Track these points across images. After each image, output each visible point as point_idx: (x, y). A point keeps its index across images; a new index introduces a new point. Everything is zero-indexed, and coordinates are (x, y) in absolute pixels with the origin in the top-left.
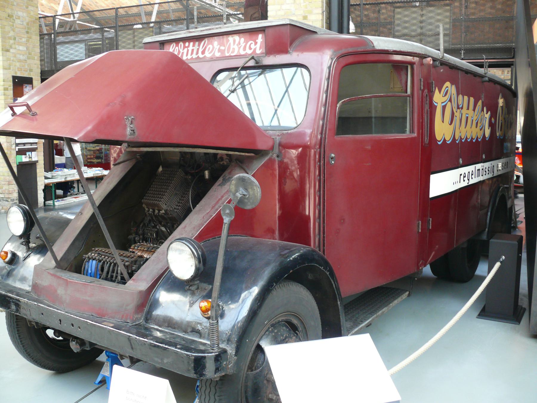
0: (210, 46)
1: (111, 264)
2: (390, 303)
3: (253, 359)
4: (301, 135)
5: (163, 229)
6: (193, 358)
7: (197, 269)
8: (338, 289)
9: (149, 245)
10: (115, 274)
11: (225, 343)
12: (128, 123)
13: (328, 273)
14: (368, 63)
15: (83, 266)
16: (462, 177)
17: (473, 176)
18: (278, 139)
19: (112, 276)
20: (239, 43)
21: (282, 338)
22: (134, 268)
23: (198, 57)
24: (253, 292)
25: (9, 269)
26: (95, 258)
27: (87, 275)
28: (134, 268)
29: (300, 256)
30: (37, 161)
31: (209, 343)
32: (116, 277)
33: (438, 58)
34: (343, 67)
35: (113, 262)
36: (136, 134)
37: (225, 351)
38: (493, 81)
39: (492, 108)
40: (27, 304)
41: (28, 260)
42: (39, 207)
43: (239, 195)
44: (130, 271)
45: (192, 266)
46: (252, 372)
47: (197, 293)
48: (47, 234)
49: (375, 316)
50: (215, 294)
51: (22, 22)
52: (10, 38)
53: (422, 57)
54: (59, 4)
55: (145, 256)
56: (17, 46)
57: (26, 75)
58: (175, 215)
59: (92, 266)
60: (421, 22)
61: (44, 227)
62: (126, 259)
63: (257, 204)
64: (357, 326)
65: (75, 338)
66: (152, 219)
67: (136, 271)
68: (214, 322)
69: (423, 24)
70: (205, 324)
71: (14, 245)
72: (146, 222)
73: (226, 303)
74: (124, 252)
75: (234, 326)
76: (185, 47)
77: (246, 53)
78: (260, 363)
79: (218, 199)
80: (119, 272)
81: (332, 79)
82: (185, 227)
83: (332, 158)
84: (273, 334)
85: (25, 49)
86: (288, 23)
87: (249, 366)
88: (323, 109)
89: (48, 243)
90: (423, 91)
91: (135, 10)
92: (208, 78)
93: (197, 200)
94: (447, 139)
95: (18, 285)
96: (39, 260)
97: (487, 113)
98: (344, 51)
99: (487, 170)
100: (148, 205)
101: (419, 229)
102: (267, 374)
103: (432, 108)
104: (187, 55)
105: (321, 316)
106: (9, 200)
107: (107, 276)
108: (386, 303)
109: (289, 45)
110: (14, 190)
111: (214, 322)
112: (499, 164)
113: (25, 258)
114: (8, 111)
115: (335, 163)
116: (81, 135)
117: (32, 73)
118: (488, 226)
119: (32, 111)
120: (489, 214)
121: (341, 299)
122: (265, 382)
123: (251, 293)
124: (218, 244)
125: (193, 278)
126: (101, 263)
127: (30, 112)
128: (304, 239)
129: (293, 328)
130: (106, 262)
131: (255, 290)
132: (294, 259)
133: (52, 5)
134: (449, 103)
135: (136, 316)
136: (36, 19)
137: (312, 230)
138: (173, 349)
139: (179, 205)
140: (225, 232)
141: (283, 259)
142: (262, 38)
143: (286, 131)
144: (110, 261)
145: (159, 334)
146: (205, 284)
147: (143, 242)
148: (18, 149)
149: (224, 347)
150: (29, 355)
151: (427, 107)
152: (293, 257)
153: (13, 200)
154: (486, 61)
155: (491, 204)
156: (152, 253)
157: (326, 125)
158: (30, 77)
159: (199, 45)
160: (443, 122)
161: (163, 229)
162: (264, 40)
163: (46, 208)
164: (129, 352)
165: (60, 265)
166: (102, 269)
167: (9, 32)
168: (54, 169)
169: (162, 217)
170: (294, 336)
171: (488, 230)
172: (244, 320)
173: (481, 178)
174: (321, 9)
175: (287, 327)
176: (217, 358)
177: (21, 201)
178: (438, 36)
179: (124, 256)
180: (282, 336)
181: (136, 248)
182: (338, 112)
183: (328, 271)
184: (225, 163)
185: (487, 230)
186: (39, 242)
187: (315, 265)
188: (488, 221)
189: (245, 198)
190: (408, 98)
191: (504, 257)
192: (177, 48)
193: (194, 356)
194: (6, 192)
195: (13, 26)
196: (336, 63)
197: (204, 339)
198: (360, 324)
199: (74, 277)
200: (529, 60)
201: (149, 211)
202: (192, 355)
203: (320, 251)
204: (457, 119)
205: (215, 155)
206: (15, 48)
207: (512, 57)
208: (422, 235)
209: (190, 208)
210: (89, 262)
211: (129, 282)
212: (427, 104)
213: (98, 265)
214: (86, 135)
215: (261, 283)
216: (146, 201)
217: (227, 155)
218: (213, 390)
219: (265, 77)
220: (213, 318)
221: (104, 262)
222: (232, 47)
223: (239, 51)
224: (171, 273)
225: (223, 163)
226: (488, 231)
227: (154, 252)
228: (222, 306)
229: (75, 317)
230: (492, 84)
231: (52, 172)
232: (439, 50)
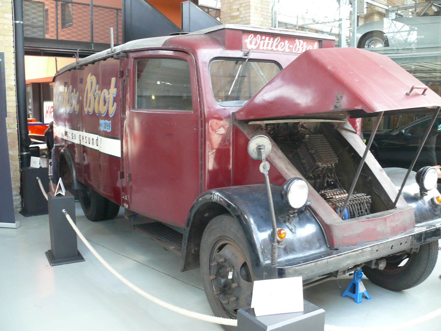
0: (282, 43)
20: (302, 46)
23: (272, 49)
76: (261, 40)
77: (278, 50)
104: (263, 46)
159: (273, 40)
192: (255, 39)
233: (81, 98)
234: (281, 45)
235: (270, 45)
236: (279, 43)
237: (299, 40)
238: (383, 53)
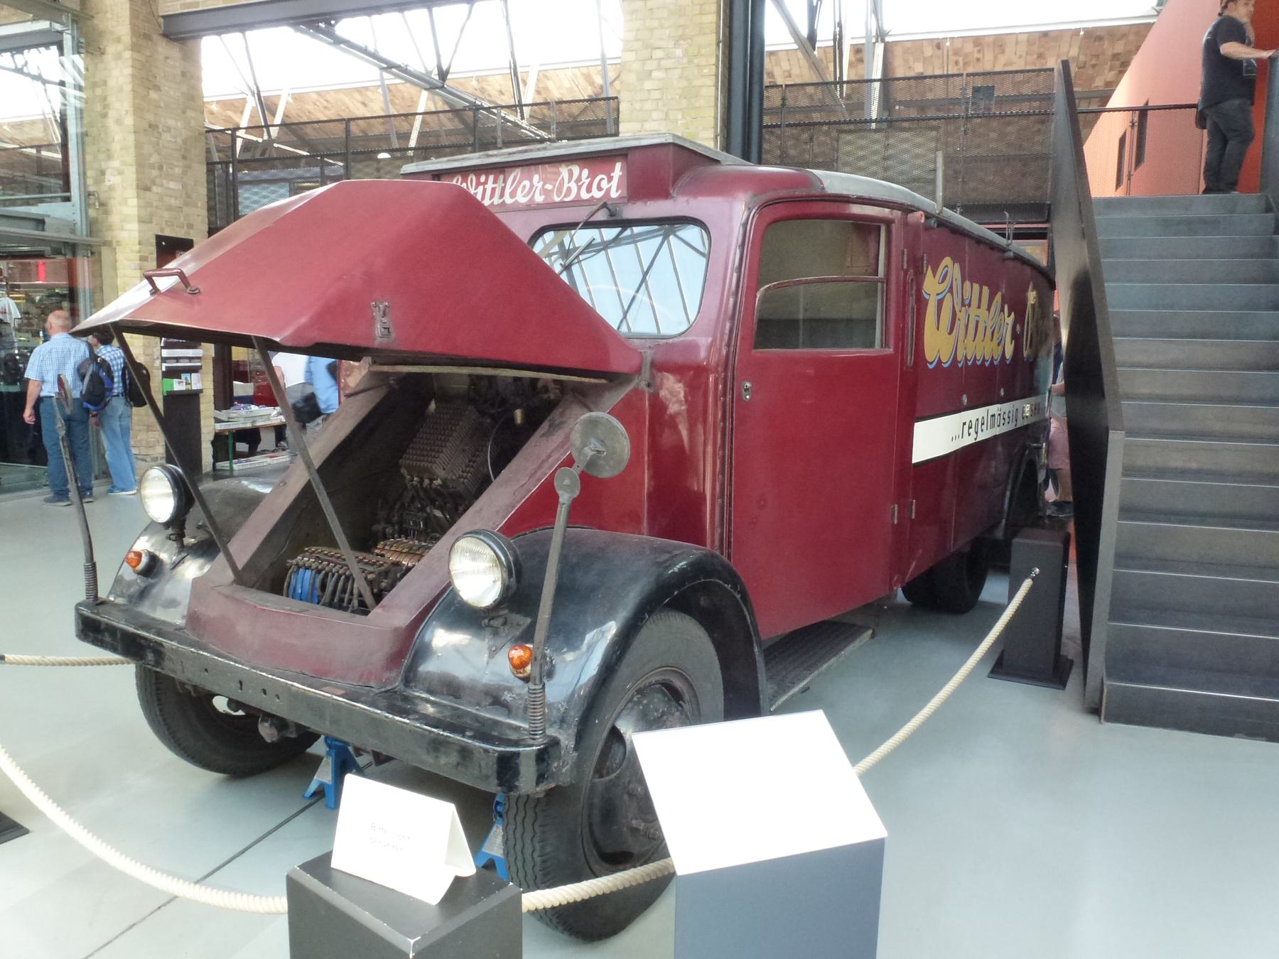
1: (340, 576)
2: (841, 650)
3: (605, 754)
4: (692, 347)
5: (438, 513)
6: (496, 755)
7: (506, 589)
8: (755, 627)
9: (411, 542)
10: (347, 596)
11: (556, 726)
12: (377, 314)
13: (738, 597)
14: (812, 218)
15: (287, 580)
16: (966, 427)
17: (984, 427)
18: (649, 355)
19: (342, 600)
20: (579, 179)
22: (383, 585)
24: (609, 630)
25: (143, 585)
26: (310, 566)
27: (288, 596)
28: (383, 585)
29: (692, 565)
30: (201, 391)
31: (526, 726)
32: (350, 601)
33: (933, 213)
34: (770, 224)
35: (344, 574)
36: (393, 335)
37: (555, 743)
38: (1020, 259)
39: (1017, 306)
40: (176, 651)
41: (181, 568)
42: (204, 472)
43: (589, 452)
44: (375, 590)
45: (495, 582)
46: (602, 779)
47: (504, 631)
48: (218, 520)
49: (816, 672)
50: (541, 633)
51: (175, 137)
52: (152, 167)
53: (907, 209)
54: (242, 112)
55: (404, 562)
56: (164, 182)
57: (180, 234)
58: (460, 489)
59: (304, 580)
60: (885, 159)
61: (213, 508)
62: (370, 568)
63: (622, 467)
64: (785, 692)
65: (268, 716)
66: (419, 495)
67: (389, 591)
68: (537, 687)
69: (890, 163)
70: (518, 691)
71: (153, 540)
72: (407, 500)
73: (558, 650)
74: (364, 554)
75: (573, 694)
76: (478, 184)
77: (592, 197)
78: (617, 761)
79: (540, 461)
80: (355, 591)
82: (481, 510)
83: (746, 390)
84: (641, 707)
85: (181, 187)
86: (671, 141)
87: (596, 767)
88: (731, 300)
89: (220, 537)
90: (906, 272)
91: (378, 129)
92: (524, 236)
93: (502, 461)
94: (944, 360)
95: (161, 614)
96: (201, 568)
97: (1009, 316)
98: (770, 195)
99: (1006, 417)
100: (409, 468)
101: (893, 519)
102: (629, 782)
103: (921, 303)
105: (723, 674)
106: (149, 459)
107: (332, 599)
108: (834, 651)
109: (671, 183)
110: (158, 442)
111: (537, 687)
112: (1026, 407)
113: (176, 565)
114: (145, 285)
115: (751, 398)
116: (288, 332)
117: (191, 231)
118: (1005, 515)
119: (190, 285)
120: (1008, 494)
121: (760, 644)
122: (626, 797)
123: (603, 633)
124: (547, 541)
125: (498, 605)
126: (321, 576)
127: (187, 287)
128: (697, 536)
129: (674, 695)
130: (330, 574)
131: (612, 629)
132: (682, 570)
133: (230, 113)
134: (949, 294)
135: (387, 675)
136: (200, 134)
137: (708, 516)
138: (458, 738)
139: (468, 469)
140: (562, 519)
141: (661, 570)
142: (621, 170)
143: (665, 341)
144: (338, 572)
145: (430, 710)
146: (518, 616)
147: (400, 537)
148: (166, 367)
149: (553, 734)
150: (179, 745)
151: (912, 302)
152: (678, 566)
153: (155, 459)
154: (1010, 228)
155: (1012, 476)
156: (417, 557)
157: (738, 329)
158: (190, 238)
159: (505, 181)
160: (938, 329)
161: (438, 513)
162: (626, 173)
163: (217, 475)
164: (372, 744)
165: (243, 578)
166: (323, 586)
167: (151, 155)
168: (232, 405)
169: (437, 491)
170: (678, 710)
171: (1007, 520)
172: (590, 685)
173: (997, 431)
174: (712, 130)
175: (665, 695)
176: (542, 757)
177: (169, 459)
178: (1043, 122)
179: (366, 563)
180: (657, 711)
181: (387, 548)
183: (739, 592)
184: (552, 397)
185: (1004, 521)
186: (202, 536)
187: (718, 581)
188: (1006, 506)
189: (599, 457)
190: (879, 284)
191: (1038, 570)
193: (497, 751)
194: (144, 443)
195: (158, 144)
196: (756, 216)
197: (515, 719)
198: (790, 688)
199: (268, 602)
200: (1083, 226)
201: (412, 480)
202: (494, 750)
203: (722, 554)
204: (960, 324)
205: (534, 381)
206: (162, 185)
207: (1044, 220)
208: (897, 530)
209: (489, 476)
210: (297, 572)
211: (375, 610)
212: (912, 295)
213: (314, 578)
214: (296, 334)
215: (624, 613)
216: (408, 462)
217: (555, 381)
218: (531, 814)
219: (607, 255)
220: (535, 680)
221: (326, 575)
222: (566, 185)
223: (578, 193)
224: (455, 593)
225: (549, 397)
226: (1006, 524)
227: (421, 556)
228: (550, 658)
229: (270, 676)
230: (1018, 265)
231: (229, 411)
232: (934, 199)
233: (1018, 328)
234: (524, 187)
235: (498, 193)
236: (520, 183)
237: (567, 166)
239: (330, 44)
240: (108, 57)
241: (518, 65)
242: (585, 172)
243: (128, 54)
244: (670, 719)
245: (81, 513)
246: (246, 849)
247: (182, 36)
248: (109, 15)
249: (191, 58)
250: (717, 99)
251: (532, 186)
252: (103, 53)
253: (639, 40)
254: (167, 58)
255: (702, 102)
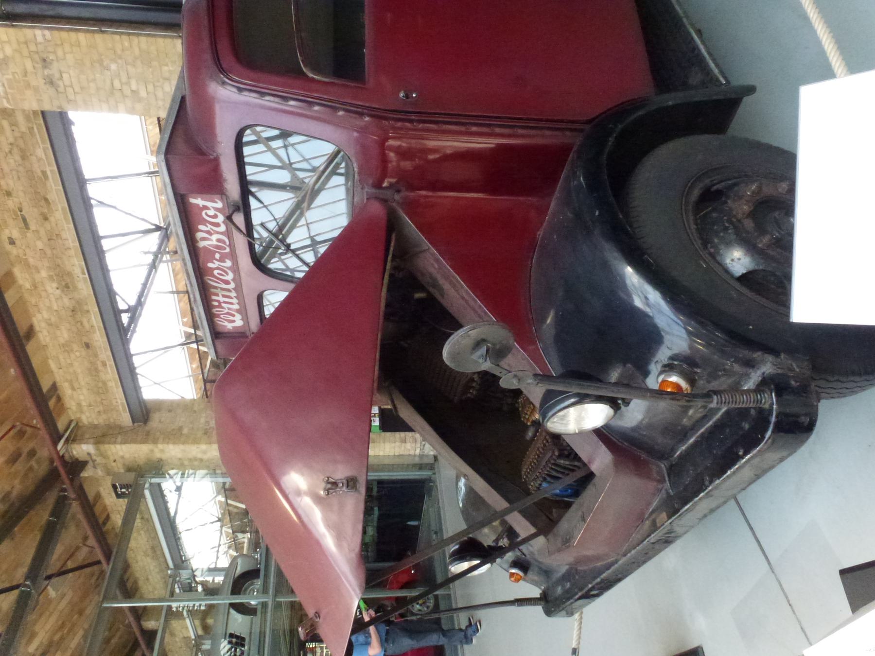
0: (216, 272)
18: (368, 189)
20: (208, 232)
21: (730, 231)
76: (220, 306)
77: (223, 222)
81: (261, 85)
83: (407, 96)
98: (208, 57)
104: (232, 303)
115: (415, 92)
159: (216, 288)
170: (726, 202)
181: (527, 417)
182: (323, 77)
221: (547, 475)
222: (215, 243)
237: (198, 242)
238: (64, 139)
239: (142, 309)
240: (164, 457)
241: (148, 170)
242: (201, 227)
243: (160, 446)
244: (734, 213)
245: (479, 608)
246: (749, 525)
247: (144, 408)
248: (136, 455)
249: (159, 405)
250: (148, 35)
251: (218, 268)
252: (161, 460)
253: (107, 100)
254: (160, 421)
255: (153, 49)
